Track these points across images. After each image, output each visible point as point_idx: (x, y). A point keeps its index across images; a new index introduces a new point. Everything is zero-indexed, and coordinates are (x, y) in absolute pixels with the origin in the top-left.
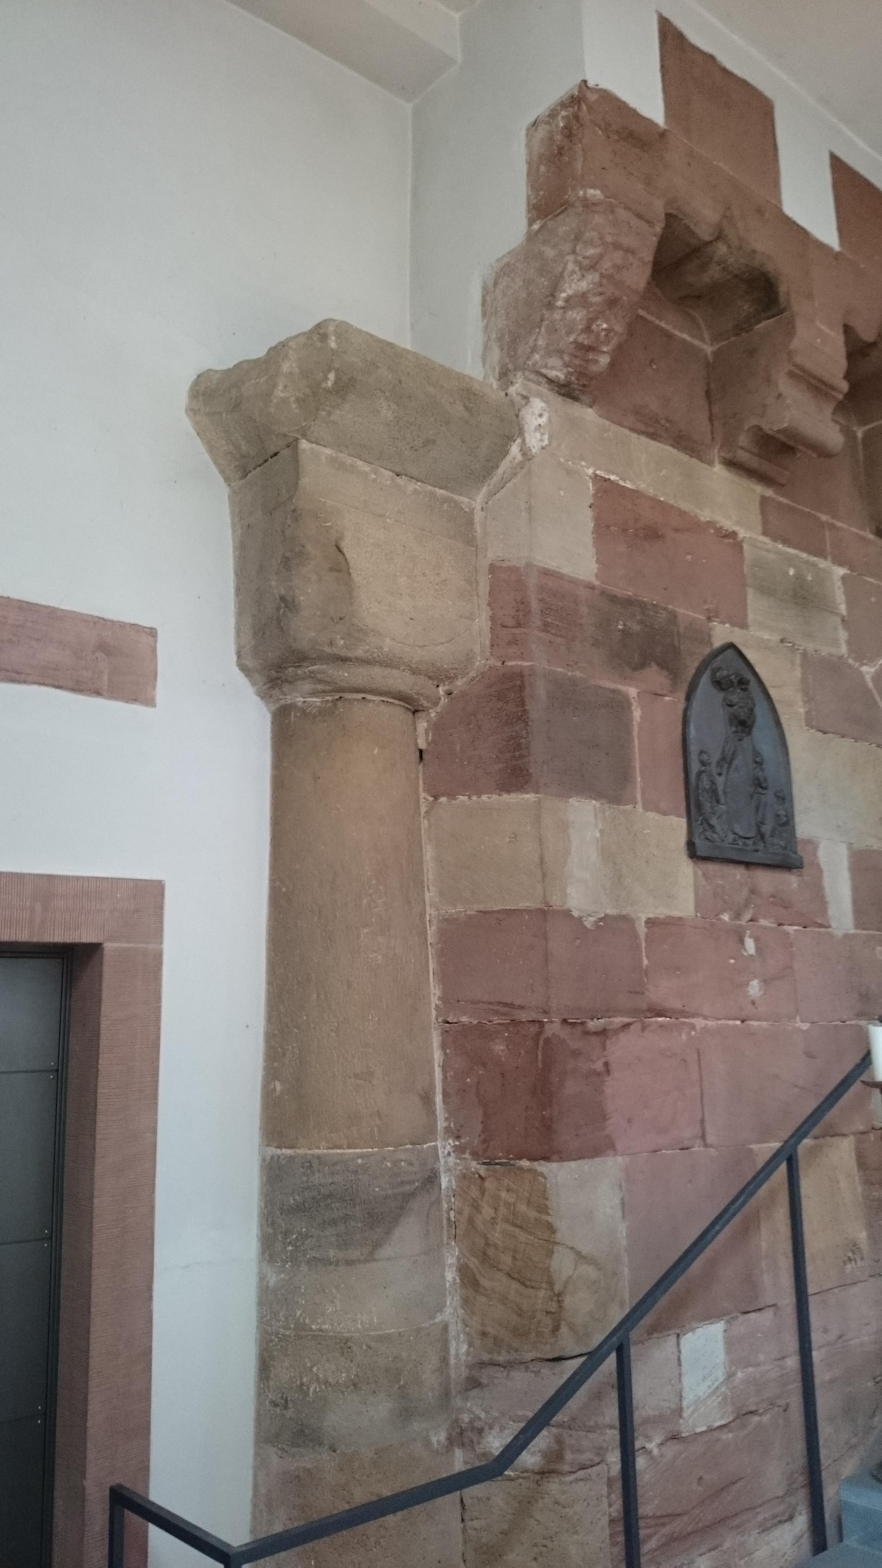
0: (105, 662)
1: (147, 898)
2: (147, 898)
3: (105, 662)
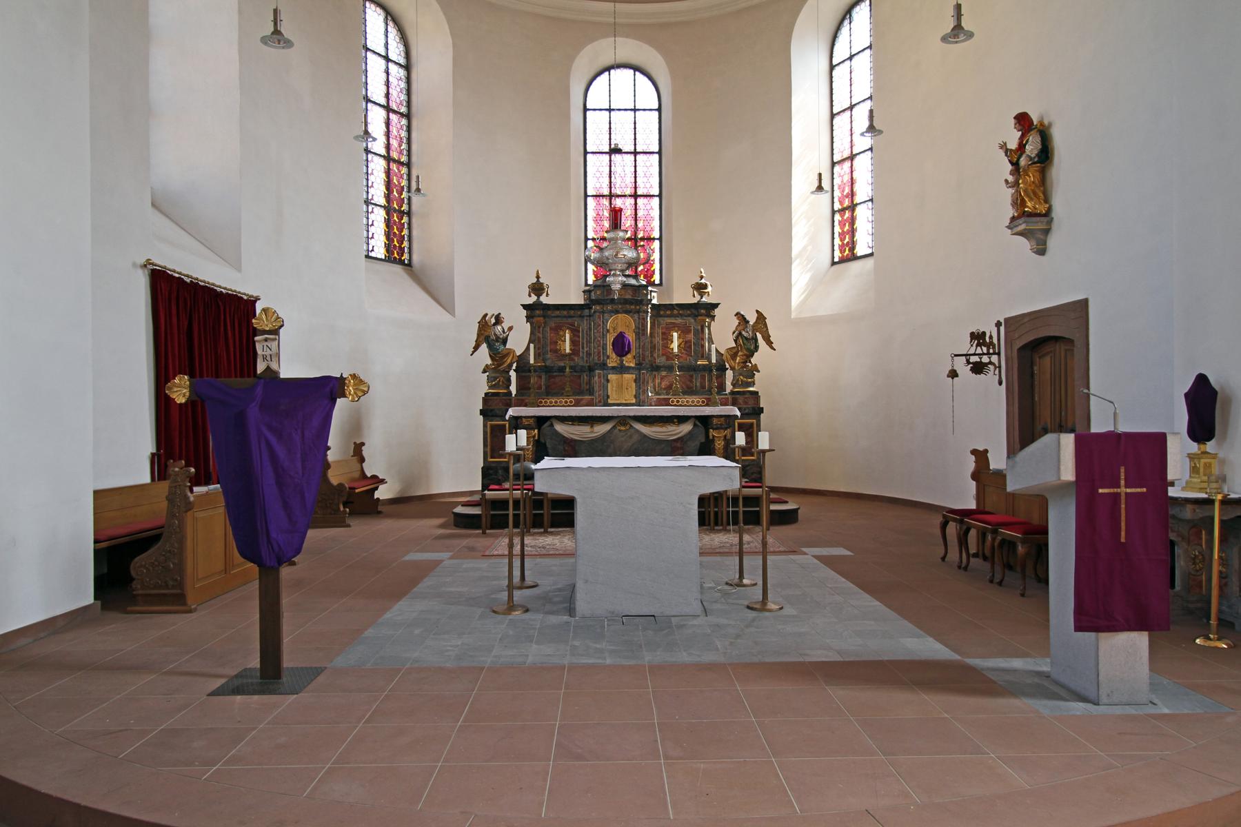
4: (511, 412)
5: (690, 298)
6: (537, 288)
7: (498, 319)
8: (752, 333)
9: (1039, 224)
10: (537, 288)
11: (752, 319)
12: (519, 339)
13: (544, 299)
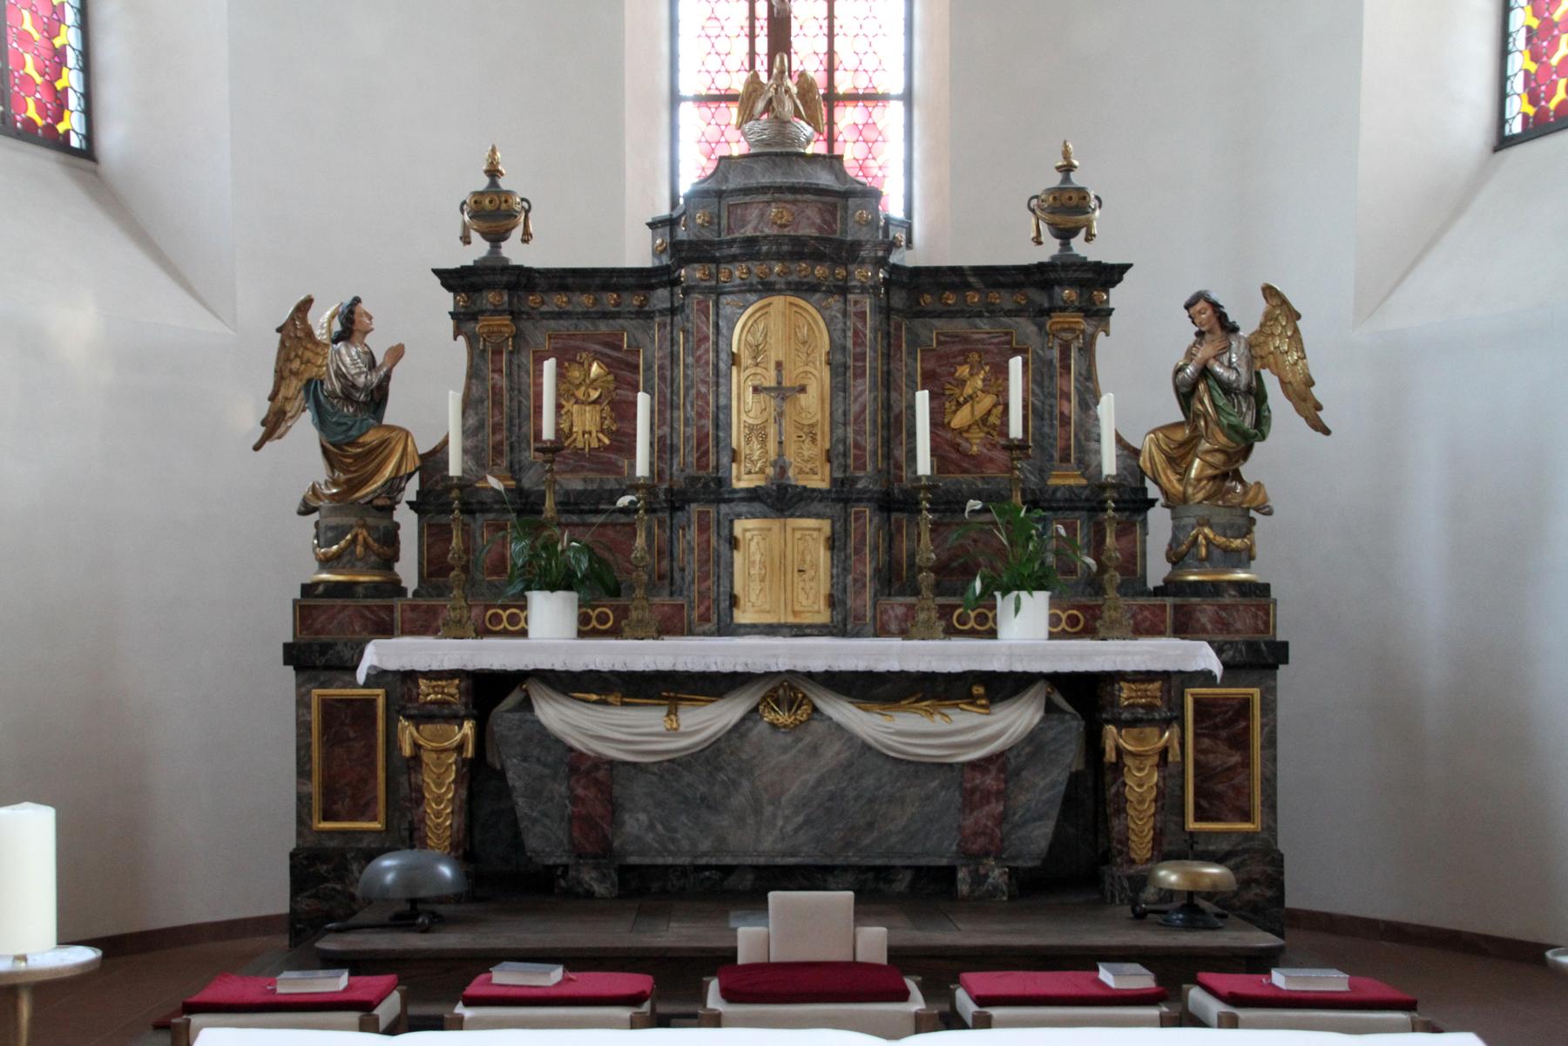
4: (378, 654)
5: (1023, 244)
6: (494, 213)
7: (350, 324)
8: (1236, 388)
10: (494, 213)
11: (1247, 314)
12: (431, 403)
13: (515, 252)
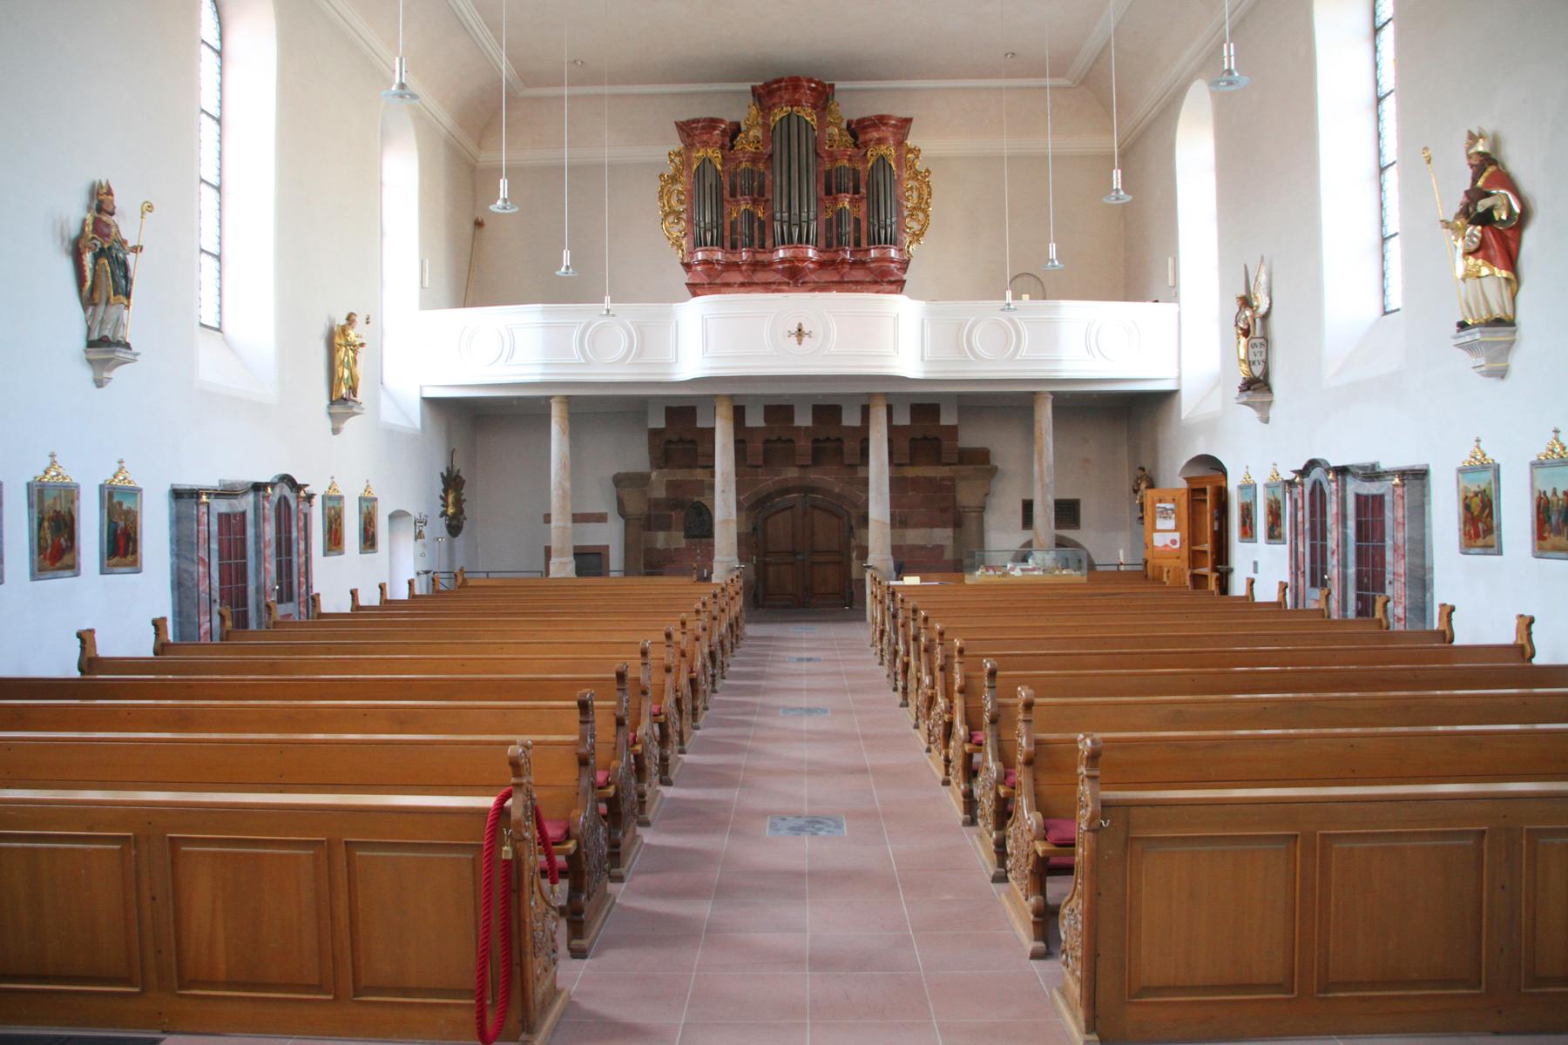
0: (601, 518)
1: (607, 547)
2: (607, 547)
3: (601, 518)
9: (1501, 334)
